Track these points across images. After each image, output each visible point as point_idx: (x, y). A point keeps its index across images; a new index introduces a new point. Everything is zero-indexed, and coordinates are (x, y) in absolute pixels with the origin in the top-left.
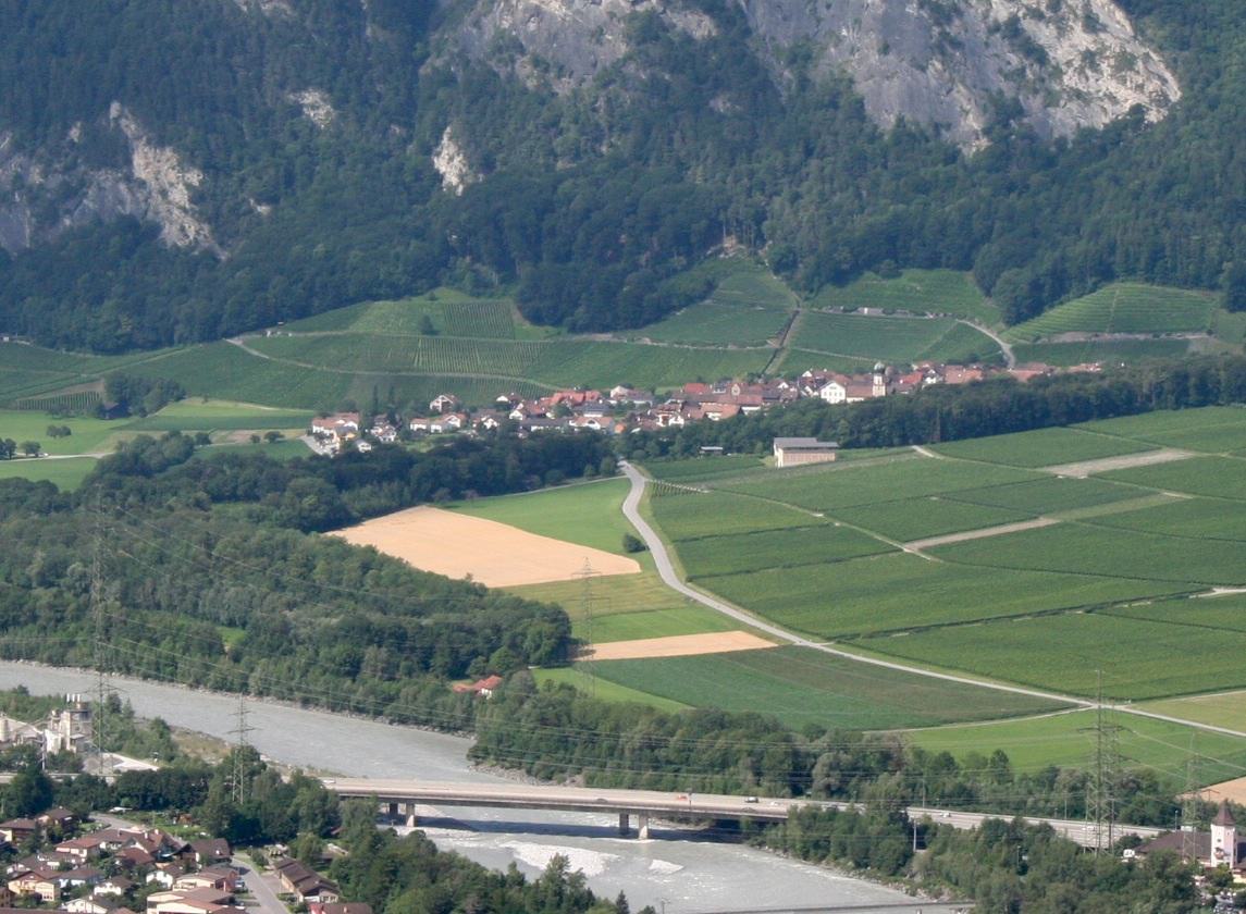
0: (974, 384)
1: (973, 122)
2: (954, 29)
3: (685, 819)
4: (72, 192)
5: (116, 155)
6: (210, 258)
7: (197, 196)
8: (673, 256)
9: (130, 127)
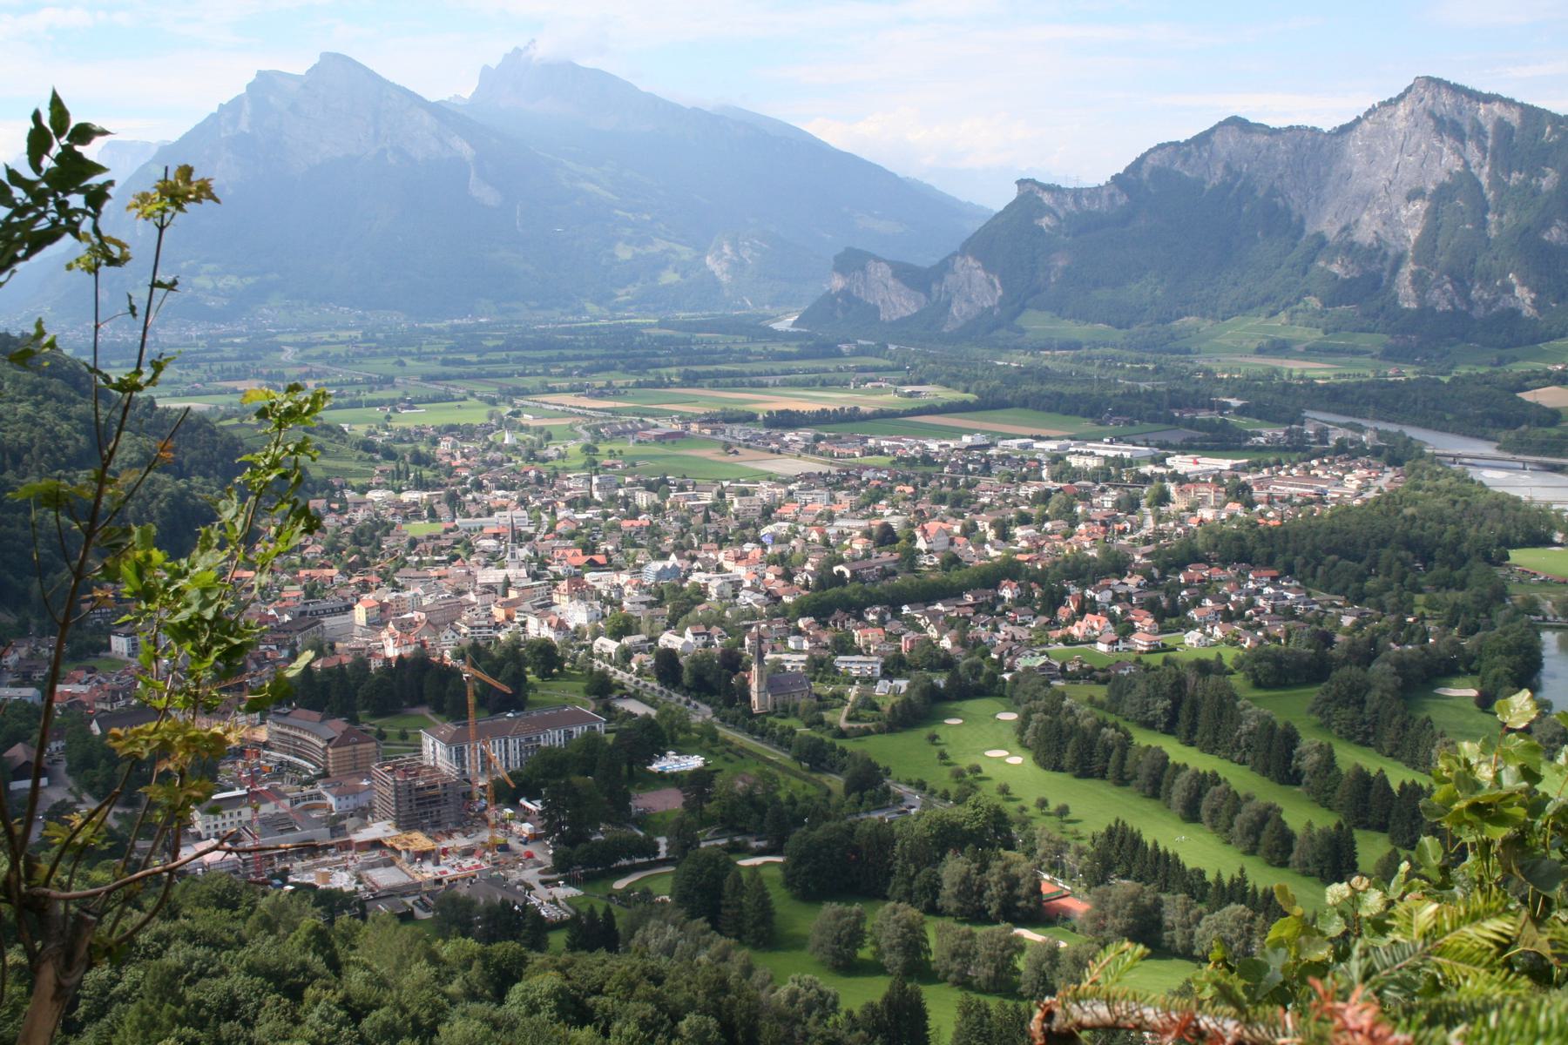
3: (753, 385)
4: (1495, 301)
6: (1536, 319)
7: (1533, 301)
8: (148, 782)
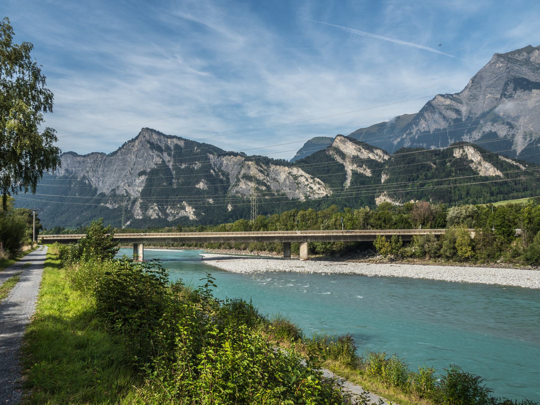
0: (496, 201)
1: (303, 198)
2: (300, 186)
4: (178, 214)
5: (183, 208)
7: (194, 212)
9: (186, 204)
